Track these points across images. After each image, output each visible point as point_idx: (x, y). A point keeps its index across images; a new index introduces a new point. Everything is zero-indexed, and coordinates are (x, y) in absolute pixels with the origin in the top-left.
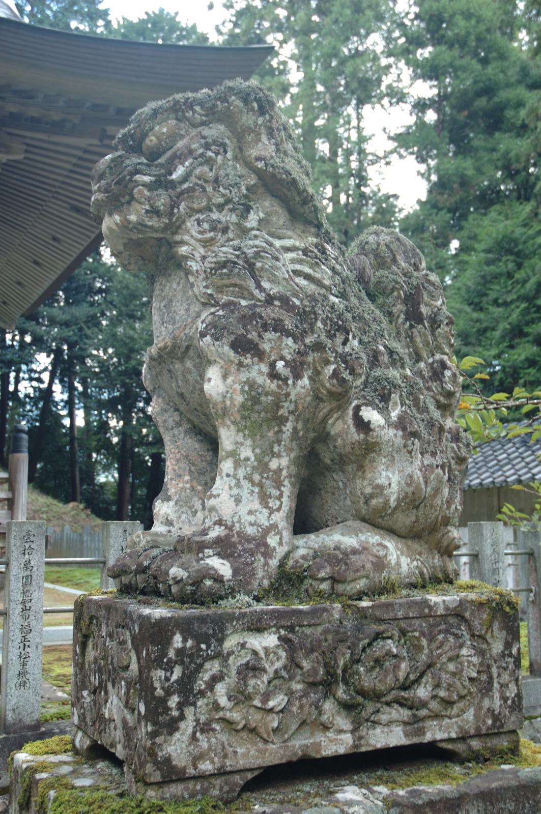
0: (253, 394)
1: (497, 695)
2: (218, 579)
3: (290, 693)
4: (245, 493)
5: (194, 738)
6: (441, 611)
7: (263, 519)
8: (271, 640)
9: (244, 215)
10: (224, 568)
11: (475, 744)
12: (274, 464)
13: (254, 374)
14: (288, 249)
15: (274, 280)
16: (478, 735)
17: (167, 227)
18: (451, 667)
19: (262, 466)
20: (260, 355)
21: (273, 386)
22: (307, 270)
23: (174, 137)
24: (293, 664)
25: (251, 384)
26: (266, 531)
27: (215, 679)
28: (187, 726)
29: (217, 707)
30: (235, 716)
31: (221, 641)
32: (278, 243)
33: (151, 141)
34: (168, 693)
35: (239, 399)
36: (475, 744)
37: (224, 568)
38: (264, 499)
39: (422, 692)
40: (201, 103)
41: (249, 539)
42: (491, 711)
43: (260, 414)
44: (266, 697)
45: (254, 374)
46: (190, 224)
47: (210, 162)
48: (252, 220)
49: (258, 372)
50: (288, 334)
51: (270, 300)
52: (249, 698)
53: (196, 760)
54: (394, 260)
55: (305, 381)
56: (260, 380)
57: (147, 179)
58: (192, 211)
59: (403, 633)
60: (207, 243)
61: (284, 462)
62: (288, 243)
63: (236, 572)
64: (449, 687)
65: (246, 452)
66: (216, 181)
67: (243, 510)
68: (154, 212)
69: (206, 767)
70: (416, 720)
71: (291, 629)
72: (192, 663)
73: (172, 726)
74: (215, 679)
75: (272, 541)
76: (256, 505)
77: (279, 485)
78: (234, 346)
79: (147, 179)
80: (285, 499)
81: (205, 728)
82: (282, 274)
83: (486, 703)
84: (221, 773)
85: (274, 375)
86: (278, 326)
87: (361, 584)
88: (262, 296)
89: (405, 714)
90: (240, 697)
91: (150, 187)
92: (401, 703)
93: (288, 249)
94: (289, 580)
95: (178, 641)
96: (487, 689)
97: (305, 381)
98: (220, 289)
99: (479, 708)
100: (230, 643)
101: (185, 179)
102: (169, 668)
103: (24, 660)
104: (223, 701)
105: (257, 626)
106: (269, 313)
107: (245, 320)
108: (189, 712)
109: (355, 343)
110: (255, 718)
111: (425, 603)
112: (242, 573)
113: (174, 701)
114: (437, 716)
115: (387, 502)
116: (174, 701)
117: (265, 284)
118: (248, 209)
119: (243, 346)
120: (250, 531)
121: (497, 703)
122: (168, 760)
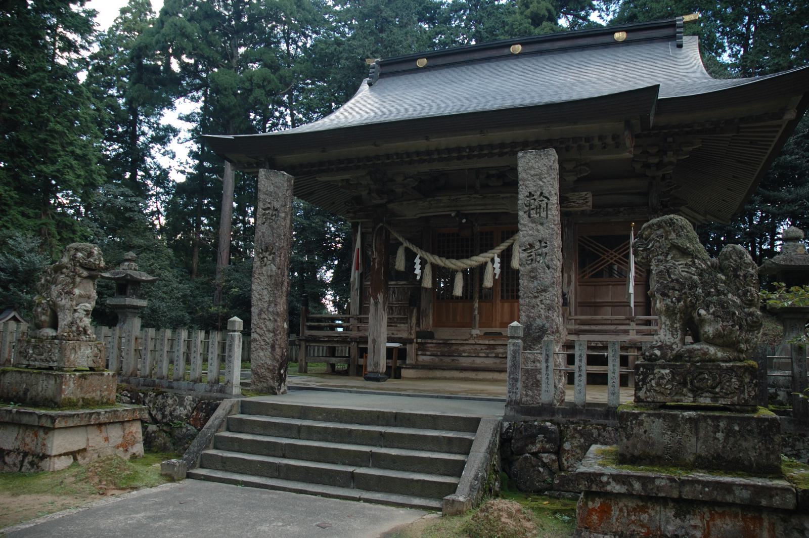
0: (668, 308)
1: (746, 394)
2: (656, 355)
3: (673, 385)
4: (667, 334)
5: (646, 393)
6: (725, 367)
7: (672, 340)
8: (667, 371)
9: (666, 257)
10: (658, 353)
11: (738, 407)
12: (675, 326)
13: (667, 302)
14: (680, 265)
15: (675, 275)
16: (738, 405)
17: (647, 261)
18: (728, 384)
19: (672, 326)
20: (669, 297)
21: (672, 305)
22: (686, 270)
23: (650, 234)
24: (673, 378)
25: (667, 304)
26: (673, 344)
27: (652, 379)
28: (644, 389)
29: (652, 386)
30: (657, 389)
31: (653, 370)
32: (677, 263)
33: (644, 236)
34: (639, 381)
35: (664, 309)
36: (738, 407)
37: (658, 353)
38: (673, 335)
39: (717, 390)
40: (656, 224)
41: (667, 346)
42: (744, 399)
43: (670, 312)
44: (665, 385)
45: (667, 302)
46: (653, 260)
47: (658, 241)
48: (669, 257)
49: (668, 301)
50: (676, 290)
51: (673, 281)
52: (661, 385)
53: (646, 398)
54: (731, 257)
55: (682, 303)
56: (669, 303)
57: (641, 249)
58: (653, 257)
59: (710, 373)
60: (657, 266)
61: (678, 325)
62: (680, 263)
63: (661, 354)
64: (727, 389)
65: (668, 323)
66: (660, 247)
67: (667, 338)
68: (643, 258)
69: (649, 400)
70: (715, 397)
71: (674, 369)
72: (646, 375)
73: (640, 389)
74: (652, 379)
75: (674, 346)
76: (670, 337)
77: (677, 331)
78: (661, 295)
79: (641, 249)
80: (679, 335)
81: (649, 391)
82: (677, 272)
83: (742, 396)
84: (653, 402)
85: (672, 302)
86: (674, 289)
87: (697, 359)
88: (670, 280)
89: (711, 395)
90: (658, 384)
91: (642, 251)
92: (710, 392)
93: (680, 265)
94: (679, 357)
95: (641, 369)
96: (743, 392)
97: (682, 303)
98: (660, 278)
99: (739, 397)
100: (656, 371)
101: (652, 247)
102: (639, 375)
103: (724, 408)
104: (654, 385)
105: (664, 367)
106: (671, 285)
107: (665, 287)
108: (645, 386)
109: (700, 291)
110: (662, 390)
111: (719, 365)
112: (663, 356)
113: (640, 383)
114: (723, 397)
115: (708, 336)
116: (640, 383)
117: (672, 276)
118: (668, 254)
119: (664, 295)
120: (668, 343)
121: (746, 396)
122: (639, 397)
